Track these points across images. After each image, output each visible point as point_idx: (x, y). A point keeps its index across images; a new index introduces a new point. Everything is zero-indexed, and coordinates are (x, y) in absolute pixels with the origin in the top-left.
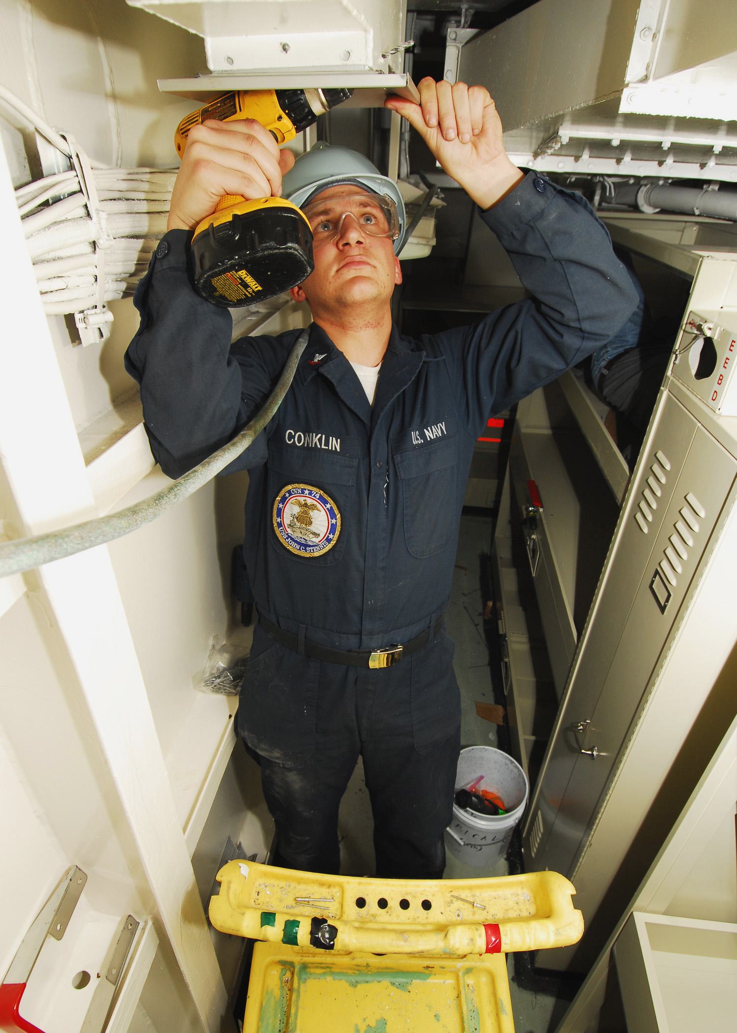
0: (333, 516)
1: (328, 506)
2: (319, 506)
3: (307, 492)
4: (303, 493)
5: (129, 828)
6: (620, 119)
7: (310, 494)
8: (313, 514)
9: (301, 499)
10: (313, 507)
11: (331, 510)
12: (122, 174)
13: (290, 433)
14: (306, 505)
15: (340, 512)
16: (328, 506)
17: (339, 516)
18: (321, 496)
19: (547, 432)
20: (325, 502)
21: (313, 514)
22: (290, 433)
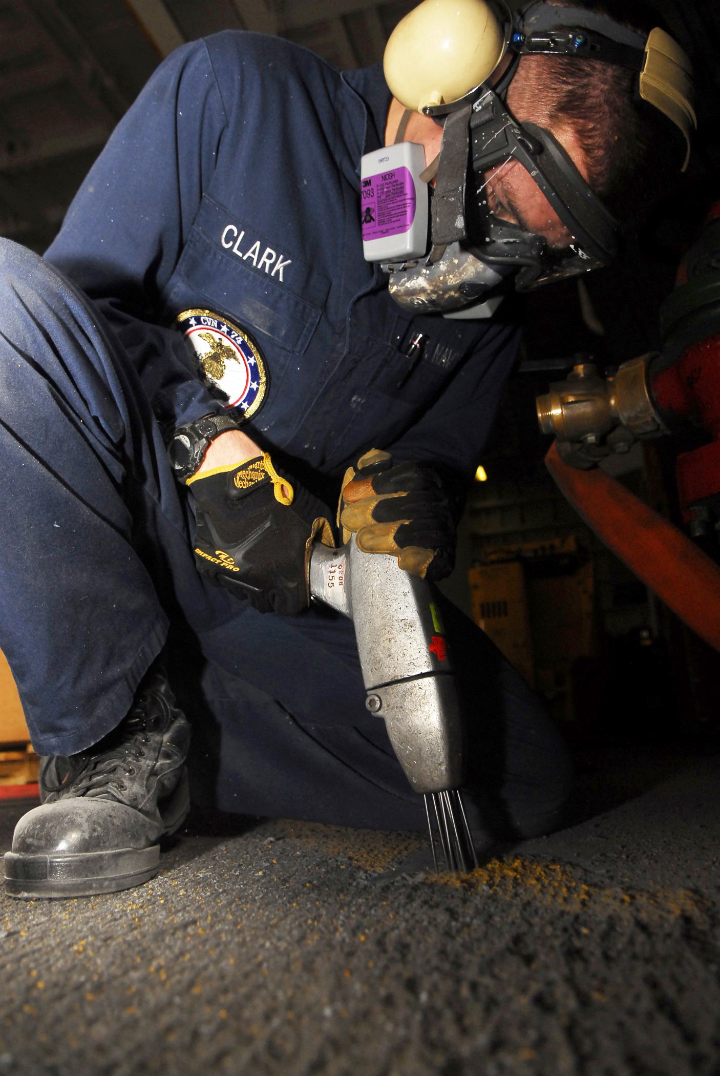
0: (255, 377)
1: (252, 361)
2: (238, 355)
3: (224, 329)
4: (219, 328)
5: (404, 116)
6: (173, 326)
7: (229, 333)
8: (228, 363)
9: (217, 336)
10: (230, 354)
11: (254, 369)
12: (432, 288)
13: (231, 231)
14: (220, 345)
15: (266, 376)
16: (252, 361)
17: (264, 379)
18: (243, 342)
19: (555, 216)
20: (249, 354)
21: (228, 363)
22: (231, 231)
